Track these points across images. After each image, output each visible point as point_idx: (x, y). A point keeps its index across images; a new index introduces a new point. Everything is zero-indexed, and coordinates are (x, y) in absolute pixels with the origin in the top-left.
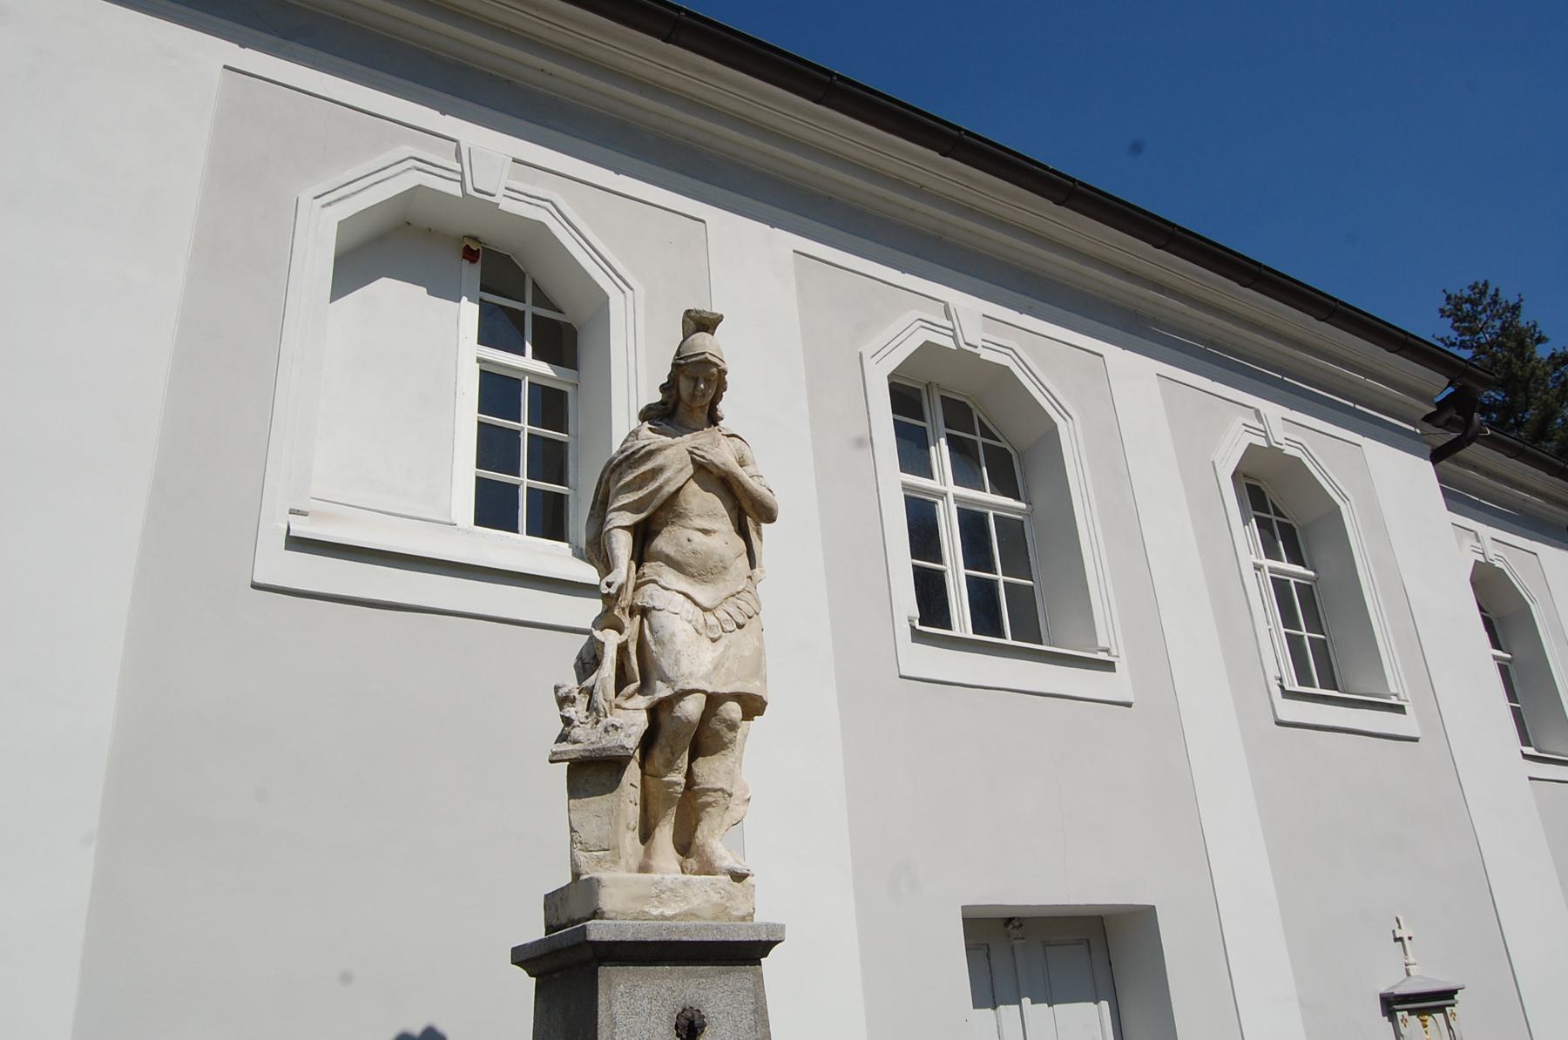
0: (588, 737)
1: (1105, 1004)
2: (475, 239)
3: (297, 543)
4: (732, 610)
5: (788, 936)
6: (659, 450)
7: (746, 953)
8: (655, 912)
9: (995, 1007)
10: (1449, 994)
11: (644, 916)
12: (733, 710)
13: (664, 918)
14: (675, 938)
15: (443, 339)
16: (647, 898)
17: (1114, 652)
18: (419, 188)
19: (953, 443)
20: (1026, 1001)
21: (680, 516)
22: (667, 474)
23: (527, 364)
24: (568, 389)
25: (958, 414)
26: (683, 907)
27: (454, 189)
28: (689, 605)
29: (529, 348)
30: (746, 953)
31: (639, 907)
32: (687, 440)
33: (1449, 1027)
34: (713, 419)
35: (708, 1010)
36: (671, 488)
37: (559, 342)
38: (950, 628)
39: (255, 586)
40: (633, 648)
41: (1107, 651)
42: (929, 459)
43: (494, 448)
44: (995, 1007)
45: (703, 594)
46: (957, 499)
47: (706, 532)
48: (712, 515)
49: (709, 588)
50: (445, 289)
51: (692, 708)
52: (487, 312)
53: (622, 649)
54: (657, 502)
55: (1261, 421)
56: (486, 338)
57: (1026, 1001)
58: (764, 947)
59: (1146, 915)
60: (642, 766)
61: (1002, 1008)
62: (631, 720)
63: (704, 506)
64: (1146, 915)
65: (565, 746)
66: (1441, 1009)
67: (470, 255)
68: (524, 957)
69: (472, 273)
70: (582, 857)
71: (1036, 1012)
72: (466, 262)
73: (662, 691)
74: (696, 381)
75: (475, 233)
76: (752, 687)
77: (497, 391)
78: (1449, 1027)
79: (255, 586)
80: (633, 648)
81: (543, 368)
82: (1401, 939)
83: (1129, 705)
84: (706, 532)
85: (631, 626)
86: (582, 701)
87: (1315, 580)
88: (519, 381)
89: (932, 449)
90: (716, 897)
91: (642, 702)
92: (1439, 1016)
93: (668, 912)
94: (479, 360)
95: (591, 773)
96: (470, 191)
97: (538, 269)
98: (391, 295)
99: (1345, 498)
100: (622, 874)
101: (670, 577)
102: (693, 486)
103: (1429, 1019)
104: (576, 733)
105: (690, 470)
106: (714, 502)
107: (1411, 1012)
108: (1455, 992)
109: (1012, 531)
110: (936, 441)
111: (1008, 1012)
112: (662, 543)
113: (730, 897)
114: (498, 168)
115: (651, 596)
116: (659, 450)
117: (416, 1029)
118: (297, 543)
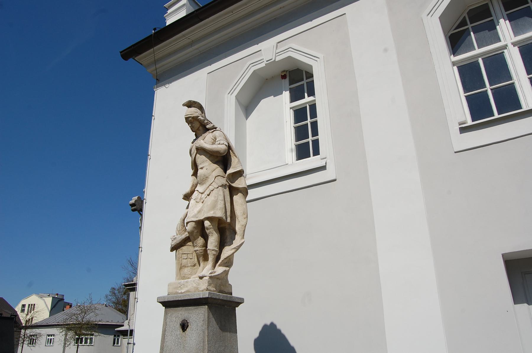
2: (284, 71)
8: (180, 292)
11: (177, 293)
13: (181, 293)
14: (177, 299)
18: (254, 72)
27: (263, 65)
29: (306, 95)
31: (175, 291)
42: (497, 33)
48: (203, 162)
50: (277, 93)
52: (291, 91)
59: (503, 255)
64: (503, 255)
67: (284, 77)
68: (238, 302)
75: (283, 70)
89: (498, 27)
90: (195, 285)
93: (183, 291)
98: (267, 104)
102: (198, 155)
106: (203, 157)
113: (199, 284)
114: (268, 51)
117: (268, 323)
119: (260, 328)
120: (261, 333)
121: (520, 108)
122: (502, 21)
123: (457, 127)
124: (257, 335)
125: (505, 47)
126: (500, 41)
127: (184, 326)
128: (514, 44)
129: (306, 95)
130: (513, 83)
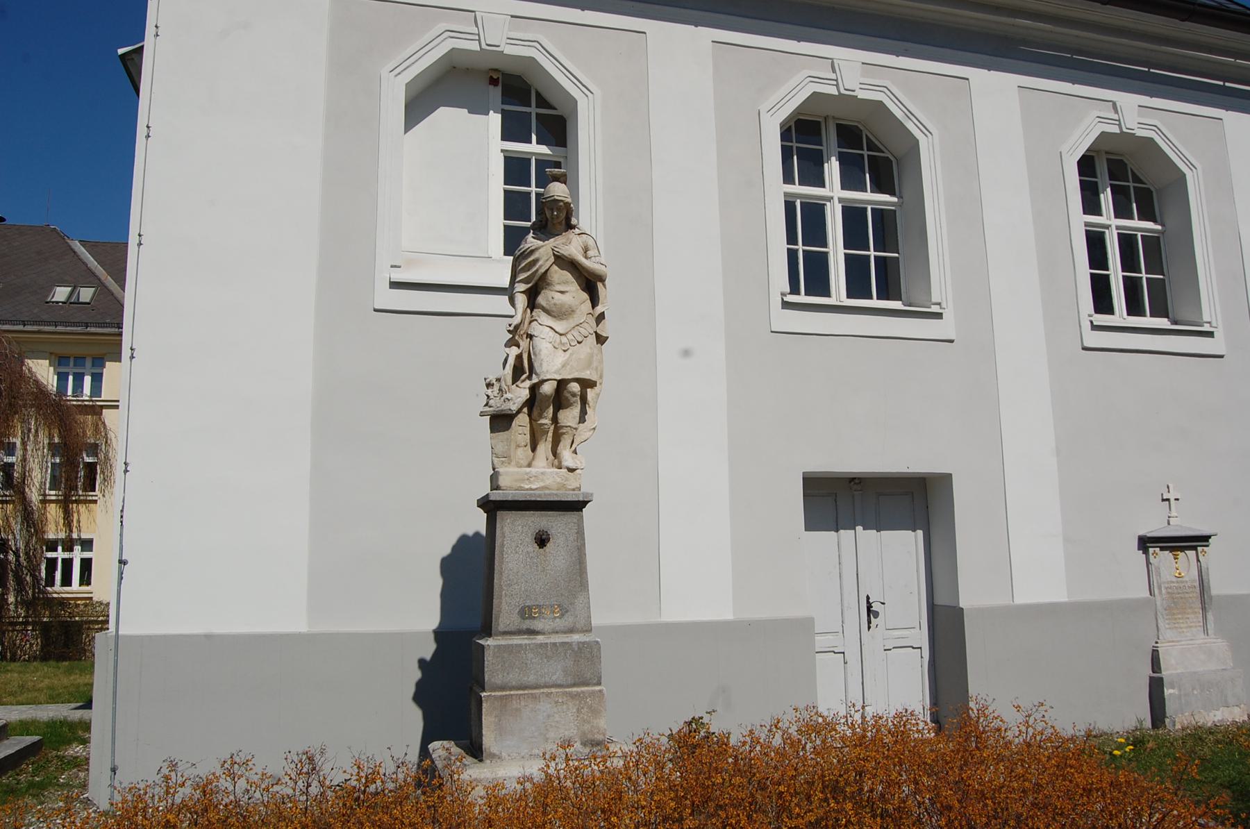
0: (498, 404)
1: (920, 533)
2: (496, 70)
3: (395, 285)
4: (576, 334)
5: (595, 498)
6: (537, 249)
7: (577, 506)
9: (837, 531)
10: (1205, 539)
11: (521, 489)
12: (575, 387)
15: (476, 141)
16: (523, 480)
17: (944, 305)
19: (842, 159)
20: (859, 528)
21: (548, 284)
22: (540, 263)
23: (534, 148)
24: (561, 160)
25: (850, 136)
26: (542, 484)
28: (552, 333)
29: (534, 137)
30: (577, 506)
32: (551, 242)
33: (1198, 560)
34: (570, 227)
35: (552, 532)
36: (542, 270)
37: (557, 128)
38: (828, 294)
39: (376, 310)
40: (525, 357)
41: (939, 304)
43: (514, 205)
44: (837, 531)
45: (560, 326)
46: (840, 200)
47: (562, 292)
48: (566, 283)
49: (564, 322)
50: (479, 108)
51: (548, 388)
52: (506, 117)
53: (519, 357)
54: (536, 278)
55: (1116, 112)
56: (505, 137)
57: (859, 528)
58: (584, 503)
59: (946, 479)
60: (530, 415)
61: (842, 531)
62: (521, 393)
63: (560, 276)
65: (487, 409)
66: (1195, 548)
67: (494, 82)
69: (496, 93)
70: (496, 460)
71: (866, 537)
72: (491, 87)
73: (535, 380)
74: (552, 210)
76: (586, 375)
77: (515, 169)
78: (1198, 560)
79: (376, 310)
80: (525, 357)
81: (544, 149)
82: (1168, 500)
83: (952, 341)
84: (562, 292)
85: (524, 343)
86: (496, 388)
87: (1162, 232)
88: (529, 160)
91: (528, 384)
92: (1191, 553)
94: (502, 151)
95: (501, 421)
96: (484, 46)
97: (537, 84)
98: (448, 118)
99: (1192, 166)
100: (512, 469)
101: (544, 318)
102: (555, 268)
103: (1181, 555)
104: (491, 402)
105: (552, 259)
106: (567, 275)
107: (1162, 549)
108: (1209, 537)
109: (884, 218)
110: (829, 159)
111: (846, 534)
112: (541, 300)
115: (535, 329)
116: (537, 249)
118: (395, 285)
119: (453, 540)
120: (455, 548)
121: (828, 294)
122: (833, 159)
123: (851, 330)
124: (447, 551)
125: (830, 199)
126: (824, 186)
127: (542, 540)
128: (840, 200)
129: (534, 137)
130: (826, 253)
